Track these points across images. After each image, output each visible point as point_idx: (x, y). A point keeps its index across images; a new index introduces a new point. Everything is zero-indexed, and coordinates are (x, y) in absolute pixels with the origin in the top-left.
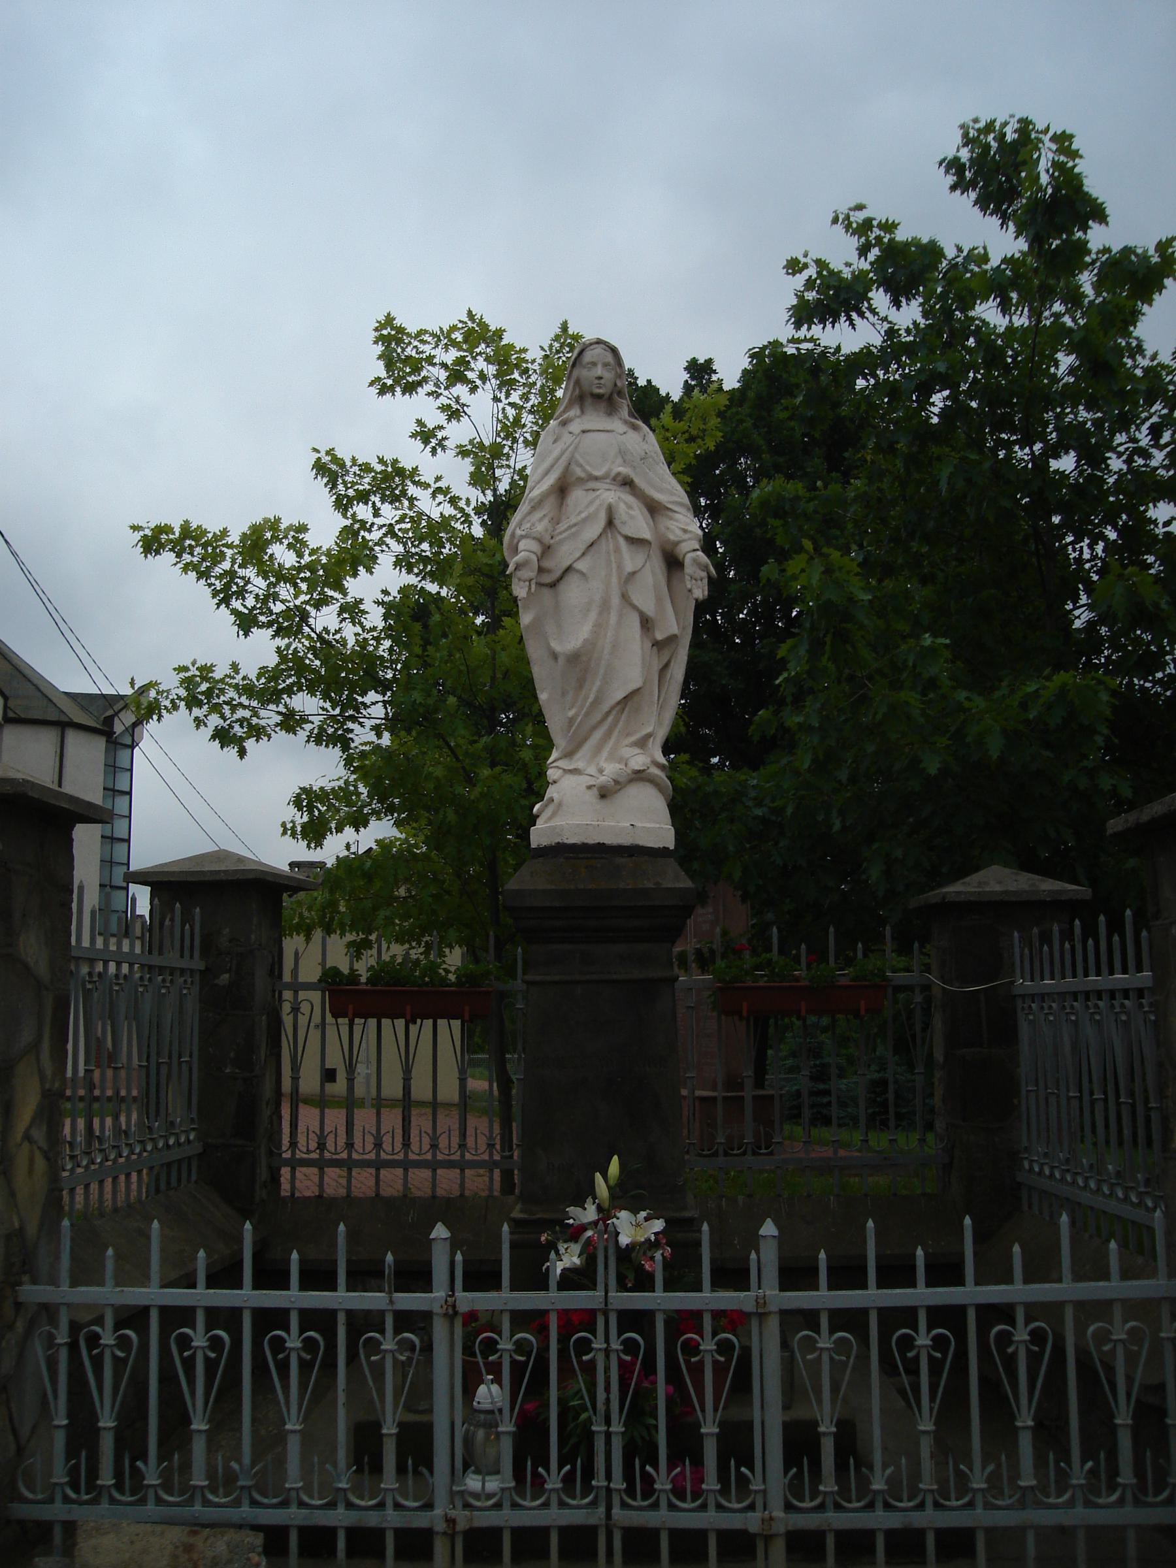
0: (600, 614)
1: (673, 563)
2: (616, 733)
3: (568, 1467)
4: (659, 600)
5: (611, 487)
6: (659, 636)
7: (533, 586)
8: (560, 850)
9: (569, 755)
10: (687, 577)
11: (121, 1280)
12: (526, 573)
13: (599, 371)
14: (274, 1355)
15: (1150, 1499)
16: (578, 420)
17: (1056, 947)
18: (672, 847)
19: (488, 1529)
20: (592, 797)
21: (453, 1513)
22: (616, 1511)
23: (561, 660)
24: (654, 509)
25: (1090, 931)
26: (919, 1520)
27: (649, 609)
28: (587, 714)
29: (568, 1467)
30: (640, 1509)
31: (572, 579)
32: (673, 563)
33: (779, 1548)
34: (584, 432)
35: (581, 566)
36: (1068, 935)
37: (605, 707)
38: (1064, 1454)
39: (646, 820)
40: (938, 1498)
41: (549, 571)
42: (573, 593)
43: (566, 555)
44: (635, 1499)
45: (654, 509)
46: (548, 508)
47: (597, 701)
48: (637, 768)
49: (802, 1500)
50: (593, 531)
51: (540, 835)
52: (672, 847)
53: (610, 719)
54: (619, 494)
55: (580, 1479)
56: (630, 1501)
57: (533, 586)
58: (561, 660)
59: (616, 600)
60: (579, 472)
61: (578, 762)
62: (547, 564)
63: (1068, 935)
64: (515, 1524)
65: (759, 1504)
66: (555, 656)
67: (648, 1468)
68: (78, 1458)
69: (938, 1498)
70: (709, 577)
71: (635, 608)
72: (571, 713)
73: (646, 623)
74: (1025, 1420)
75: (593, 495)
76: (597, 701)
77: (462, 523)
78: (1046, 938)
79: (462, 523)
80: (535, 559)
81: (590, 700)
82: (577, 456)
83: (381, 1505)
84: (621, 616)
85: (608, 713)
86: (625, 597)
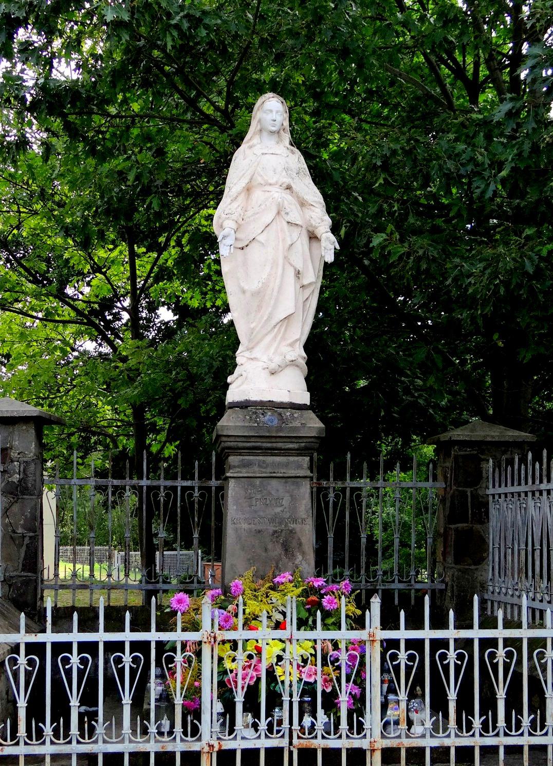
0: (272, 268)
1: (313, 237)
2: (279, 338)
3: (485, 717)
4: (305, 261)
5: (279, 190)
6: (305, 282)
7: (232, 249)
8: (244, 405)
9: (250, 349)
10: (323, 248)
11: (81, 629)
12: (229, 241)
13: (274, 116)
14: (63, 666)
15: (513, 733)
16: (259, 146)
17: (516, 467)
18: (309, 404)
19: (229, 750)
20: (265, 374)
21: (212, 743)
22: (295, 741)
23: (248, 295)
24: (303, 204)
25: (538, 458)
26: (447, 742)
27: (299, 266)
28: (262, 327)
29: (485, 717)
30: (308, 739)
31: (254, 244)
32: (313, 237)
33: (378, 756)
34: (263, 154)
35: (261, 238)
36: (523, 460)
37: (273, 322)
38: (520, 712)
39: (292, 388)
40: (105, 737)
41: (241, 240)
42: (255, 252)
43: (253, 229)
44: (32, 740)
45: (303, 204)
46: (242, 198)
47: (270, 318)
48: (291, 359)
49: (536, 731)
50: (269, 217)
51: (233, 395)
52: (309, 404)
53: (276, 330)
54: (284, 195)
55: (465, 726)
56: (460, 734)
57: (232, 249)
58: (248, 295)
59: (281, 261)
60: (260, 180)
61: (257, 353)
62: (239, 235)
63: (523, 460)
64: (457, 745)
65: (368, 735)
66: (244, 292)
67: (145, 722)
68: (536, 714)
69: (105, 737)
70: (335, 249)
71: (291, 265)
72: (252, 326)
73: (298, 273)
74: (127, 700)
75: (267, 194)
76: (270, 318)
77: (402, 241)
78: (510, 462)
79: (402, 241)
80: (233, 231)
81: (265, 318)
82: (259, 170)
83: (70, 742)
84: (284, 269)
85: (275, 326)
86: (285, 258)
